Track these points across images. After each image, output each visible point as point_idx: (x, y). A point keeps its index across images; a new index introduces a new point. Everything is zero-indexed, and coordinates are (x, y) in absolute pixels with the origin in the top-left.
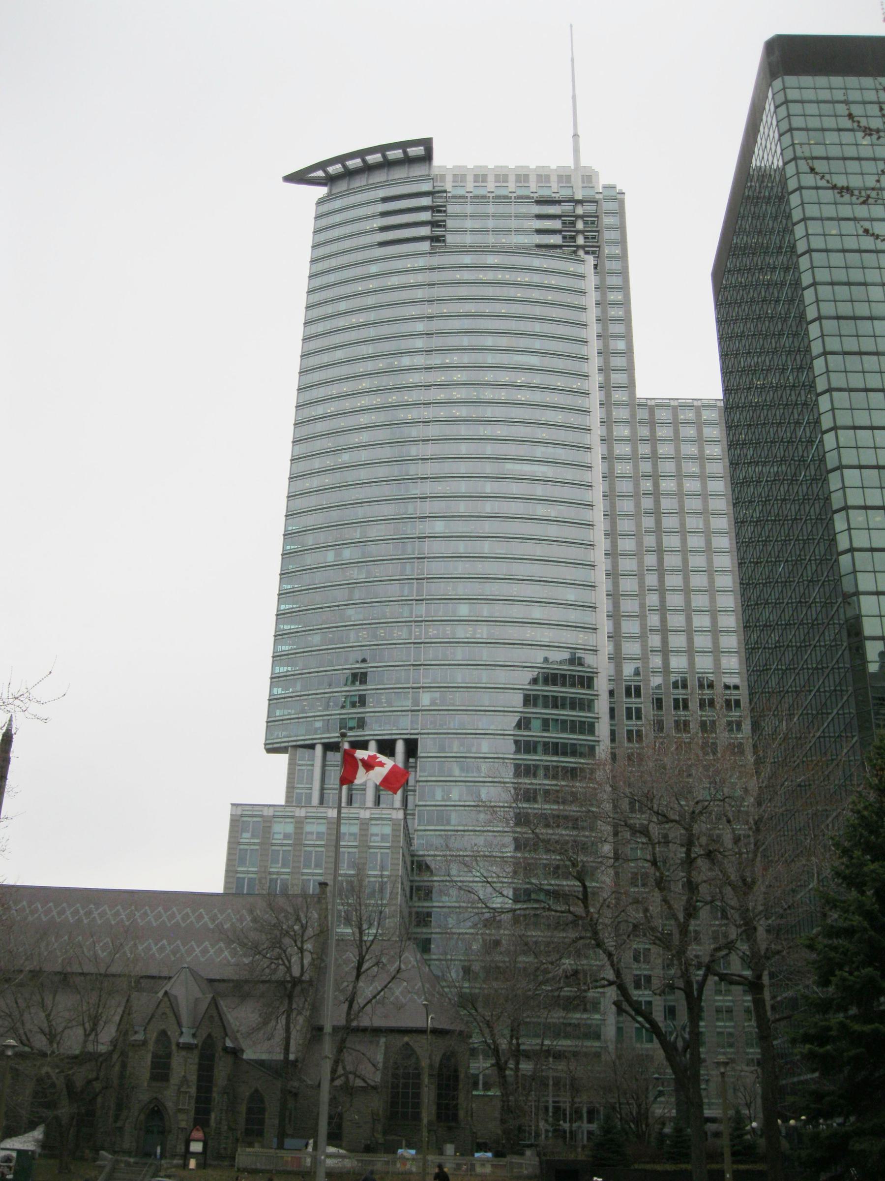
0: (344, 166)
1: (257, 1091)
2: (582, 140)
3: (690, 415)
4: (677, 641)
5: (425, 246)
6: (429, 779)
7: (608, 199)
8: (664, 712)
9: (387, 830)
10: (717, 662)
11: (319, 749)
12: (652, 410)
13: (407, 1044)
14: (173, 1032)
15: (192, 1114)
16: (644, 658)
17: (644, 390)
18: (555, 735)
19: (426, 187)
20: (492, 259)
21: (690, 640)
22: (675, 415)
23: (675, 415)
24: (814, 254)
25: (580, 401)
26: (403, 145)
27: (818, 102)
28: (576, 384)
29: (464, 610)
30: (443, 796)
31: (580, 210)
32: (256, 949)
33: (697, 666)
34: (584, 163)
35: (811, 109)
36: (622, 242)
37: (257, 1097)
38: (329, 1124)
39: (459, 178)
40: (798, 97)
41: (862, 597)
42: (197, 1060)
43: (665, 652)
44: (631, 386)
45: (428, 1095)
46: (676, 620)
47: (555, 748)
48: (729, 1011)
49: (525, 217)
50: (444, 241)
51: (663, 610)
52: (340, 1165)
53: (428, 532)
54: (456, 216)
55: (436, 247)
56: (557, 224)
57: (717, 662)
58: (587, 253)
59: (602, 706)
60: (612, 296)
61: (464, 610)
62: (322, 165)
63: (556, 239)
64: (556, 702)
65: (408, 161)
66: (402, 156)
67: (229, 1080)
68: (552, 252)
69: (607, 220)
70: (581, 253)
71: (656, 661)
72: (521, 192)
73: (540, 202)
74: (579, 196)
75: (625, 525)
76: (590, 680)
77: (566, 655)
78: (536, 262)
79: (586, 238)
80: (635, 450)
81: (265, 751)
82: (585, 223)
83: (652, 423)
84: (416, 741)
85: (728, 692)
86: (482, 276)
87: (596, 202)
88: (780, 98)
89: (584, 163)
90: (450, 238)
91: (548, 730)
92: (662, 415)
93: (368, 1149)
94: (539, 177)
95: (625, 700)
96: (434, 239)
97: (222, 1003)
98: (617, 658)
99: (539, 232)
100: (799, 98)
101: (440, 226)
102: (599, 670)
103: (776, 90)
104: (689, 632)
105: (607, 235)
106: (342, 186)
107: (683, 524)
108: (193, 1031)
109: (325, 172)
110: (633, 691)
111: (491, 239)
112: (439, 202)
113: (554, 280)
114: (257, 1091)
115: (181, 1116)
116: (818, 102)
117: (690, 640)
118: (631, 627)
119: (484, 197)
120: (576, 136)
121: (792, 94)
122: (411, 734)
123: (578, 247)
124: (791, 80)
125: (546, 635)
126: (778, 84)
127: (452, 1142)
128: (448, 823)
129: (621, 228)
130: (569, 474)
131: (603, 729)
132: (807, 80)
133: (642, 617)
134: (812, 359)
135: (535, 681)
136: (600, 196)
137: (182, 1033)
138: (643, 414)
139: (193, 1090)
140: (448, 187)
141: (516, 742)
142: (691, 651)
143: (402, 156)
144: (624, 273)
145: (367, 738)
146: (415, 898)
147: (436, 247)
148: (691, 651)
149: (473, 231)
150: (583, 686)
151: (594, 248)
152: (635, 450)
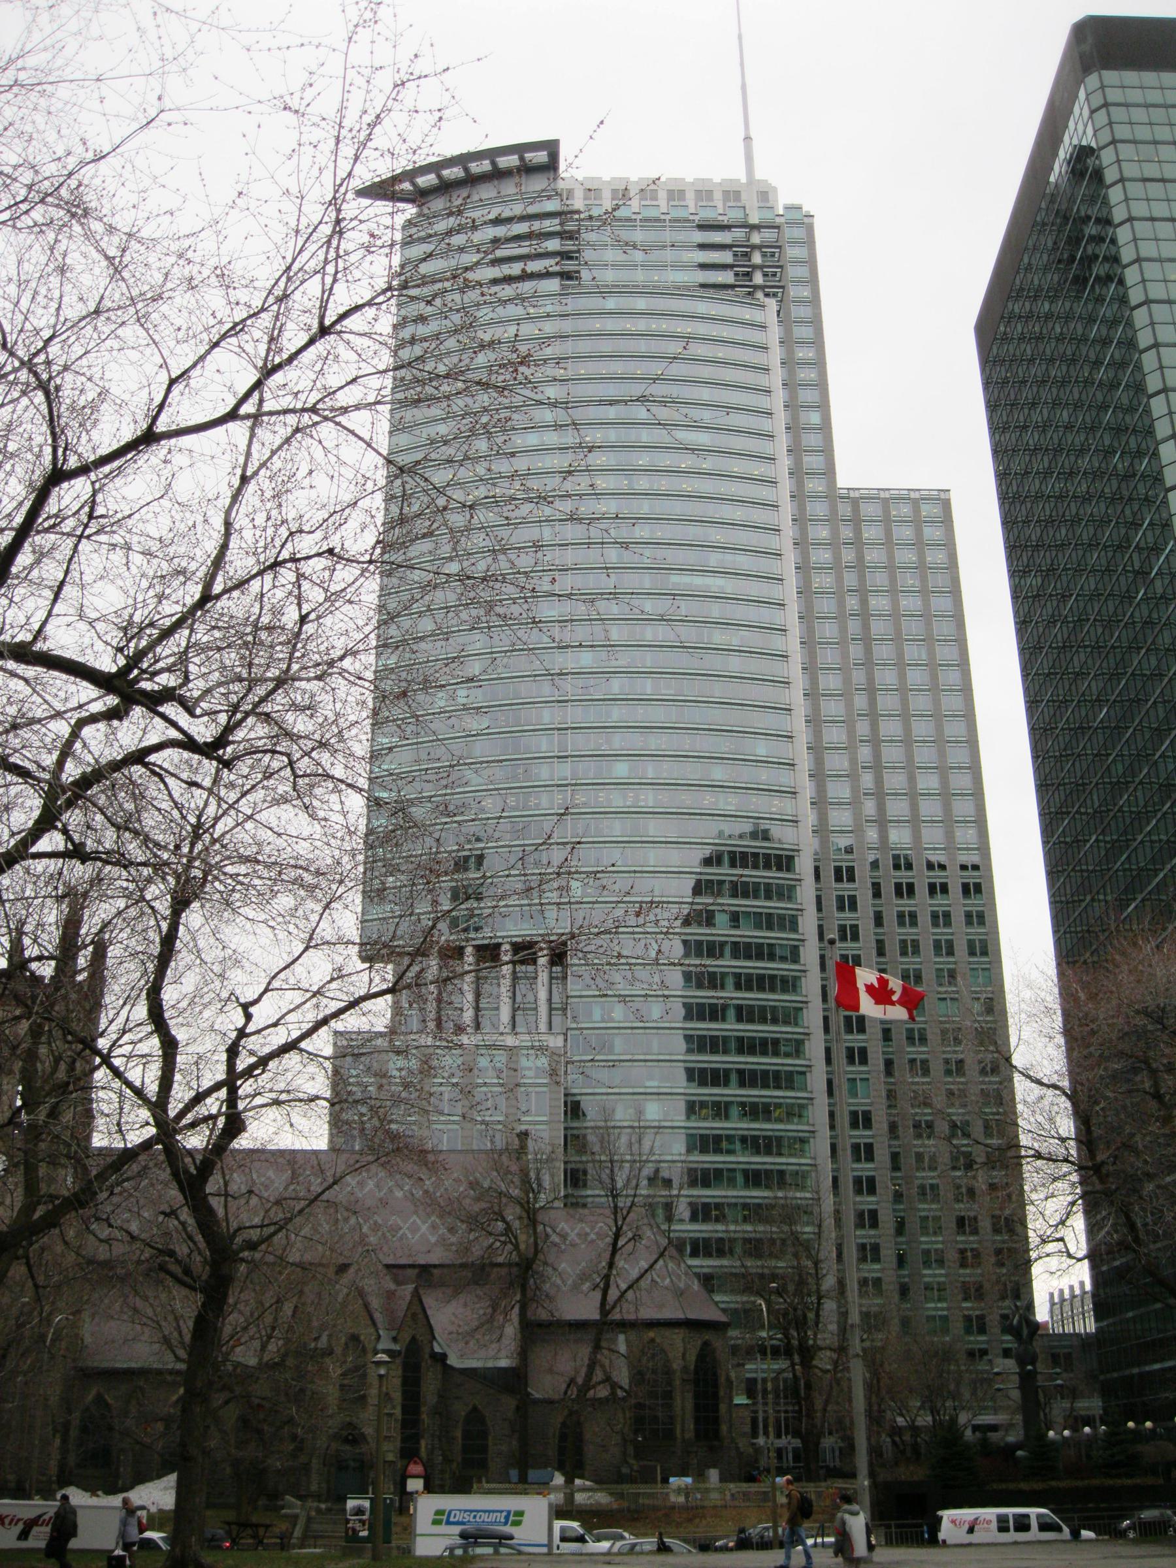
0: (439, 176)
1: (475, 1409)
2: (756, 145)
3: (906, 510)
4: (897, 808)
5: (553, 285)
7: (792, 223)
8: (883, 901)
10: (950, 835)
12: (855, 503)
13: (653, 1340)
14: (366, 1334)
15: (398, 1444)
16: (857, 830)
17: (845, 478)
18: (748, 933)
19: (551, 206)
20: (641, 304)
21: (914, 807)
22: (887, 511)
23: (887, 511)
24: (1153, 306)
25: (763, 493)
26: (520, 149)
27: (1147, 106)
29: (621, 769)
31: (756, 239)
32: (473, 1222)
33: (924, 840)
34: (759, 175)
35: (1139, 114)
36: (813, 281)
37: (475, 1417)
38: (869, 1439)
39: (591, 192)
40: (1121, 100)
42: (400, 1372)
43: (882, 822)
44: (829, 471)
45: (684, 1404)
46: (895, 781)
47: (742, 950)
48: (941, 1288)
49: (685, 246)
50: (579, 278)
51: (877, 766)
52: (592, 1501)
53: (570, 666)
54: (593, 246)
55: (569, 286)
56: (726, 257)
57: (950, 835)
58: (767, 295)
59: (806, 893)
60: (801, 353)
61: (621, 769)
62: (410, 175)
63: (727, 277)
64: (741, 890)
65: (528, 170)
66: (517, 163)
67: (440, 1396)
68: (722, 294)
69: (791, 252)
70: (759, 295)
71: (872, 834)
72: (675, 214)
73: (703, 227)
74: (754, 219)
75: (828, 656)
76: (790, 859)
77: (747, 827)
78: (702, 307)
79: (765, 275)
80: (837, 558)
82: (764, 255)
83: (856, 521)
85: (965, 873)
86: (629, 325)
87: (778, 227)
88: (1097, 100)
89: (759, 175)
90: (585, 275)
91: (737, 927)
92: (869, 510)
93: (620, 1479)
94: (698, 192)
95: (834, 885)
96: (566, 276)
97: (421, 1292)
98: (821, 830)
99: (704, 266)
100: (1161, 101)
101: (571, 258)
103: (1090, 89)
104: (913, 795)
105: (793, 272)
106: (438, 204)
107: (900, 655)
108: (394, 1333)
109: (414, 184)
110: (844, 874)
111: (640, 276)
112: (570, 226)
113: (725, 332)
114: (475, 1409)
115: (386, 1446)
116: (1147, 106)
117: (914, 807)
118: (839, 790)
119: (657, 220)
120: (748, 139)
121: (1114, 95)
123: (756, 287)
124: (1110, 76)
125: (729, 802)
126: (1092, 80)
127: (714, 1467)
128: (611, 1053)
129: (811, 262)
130: (755, 589)
131: (808, 923)
132: (1131, 77)
133: (853, 776)
134: (1158, 444)
135: (707, 862)
136: (782, 220)
137: (379, 1337)
138: (844, 510)
139: (398, 1411)
140: (578, 203)
142: (915, 821)
143: (517, 163)
144: (816, 322)
146: (570, 1150)
147: (569, 286)
148: (915, 821)
149: (615, 266)
150: (779, 869)
151: (776, 288)
152: (837, 558)
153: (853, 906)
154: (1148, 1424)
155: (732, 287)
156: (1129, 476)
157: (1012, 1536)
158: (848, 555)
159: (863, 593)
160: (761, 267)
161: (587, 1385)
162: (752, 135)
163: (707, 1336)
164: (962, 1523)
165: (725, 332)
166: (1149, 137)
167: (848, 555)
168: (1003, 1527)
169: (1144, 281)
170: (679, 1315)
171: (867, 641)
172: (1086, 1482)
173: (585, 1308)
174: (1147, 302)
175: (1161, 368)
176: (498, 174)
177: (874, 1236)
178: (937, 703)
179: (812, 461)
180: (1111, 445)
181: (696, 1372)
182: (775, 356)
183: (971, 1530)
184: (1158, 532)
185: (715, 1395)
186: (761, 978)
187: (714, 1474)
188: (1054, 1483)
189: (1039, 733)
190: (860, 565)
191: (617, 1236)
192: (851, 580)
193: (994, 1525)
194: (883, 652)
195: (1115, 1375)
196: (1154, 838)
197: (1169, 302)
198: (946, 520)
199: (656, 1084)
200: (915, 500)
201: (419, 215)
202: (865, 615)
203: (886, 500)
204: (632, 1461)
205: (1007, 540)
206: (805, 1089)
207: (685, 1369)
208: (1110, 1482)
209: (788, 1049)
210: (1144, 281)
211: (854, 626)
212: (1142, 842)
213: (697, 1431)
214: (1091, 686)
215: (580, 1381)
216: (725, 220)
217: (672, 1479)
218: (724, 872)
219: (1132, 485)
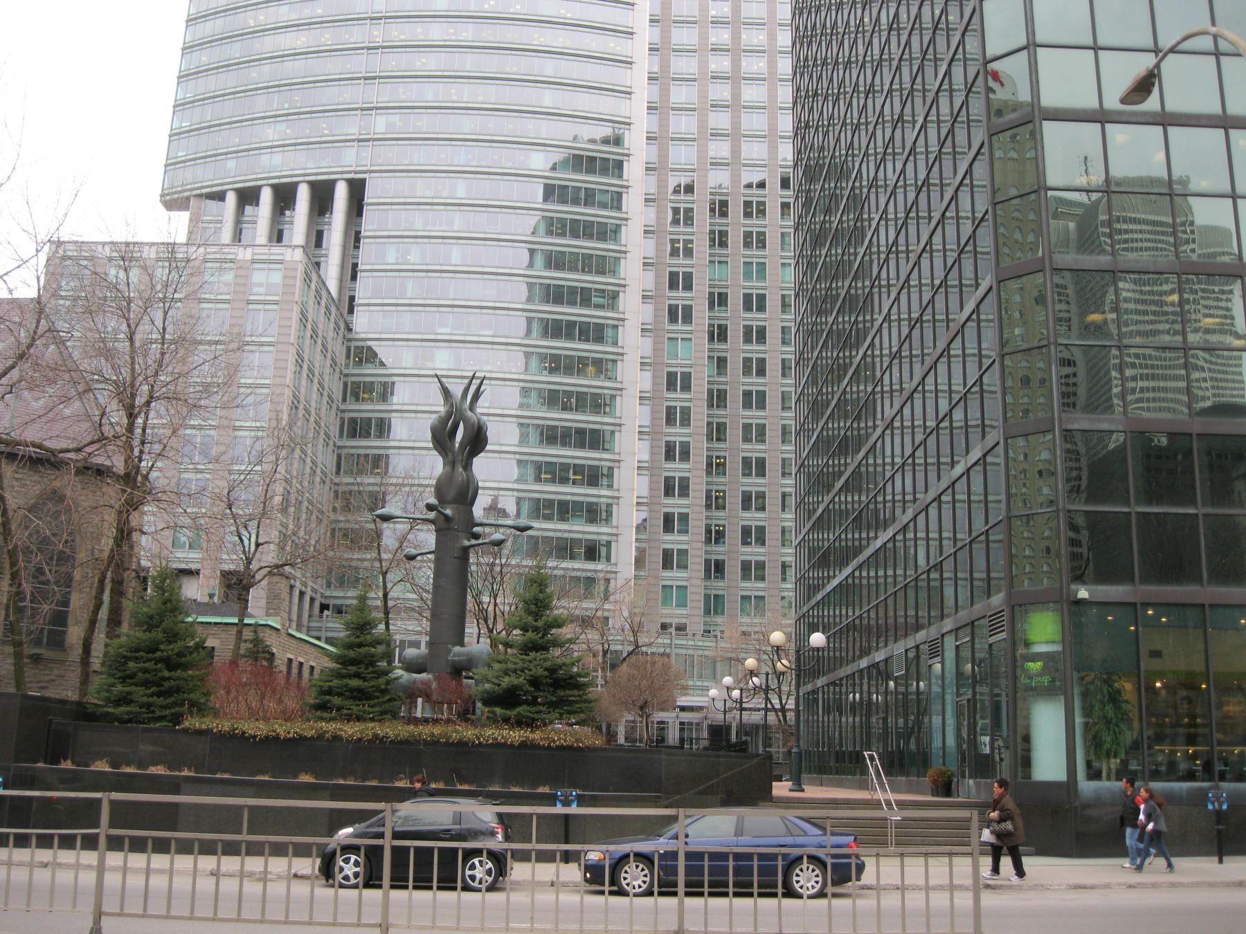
6: (378, 233)
9: (276, 277)
11: (231, 198)
28: (613, 45)
30: (397, 258)
41: (1039, 50)
81: (164, 209)
84: (363, 181)
102: (630, 184)
122: (356, 173)
141: (530, 286)
145: (295, 179)
153: (689, 220)
177: (681, 616)
186: (573, 291)
197: (1226, 123)
199: (448, 330)
206: (615, 343)
209: (600, 301)
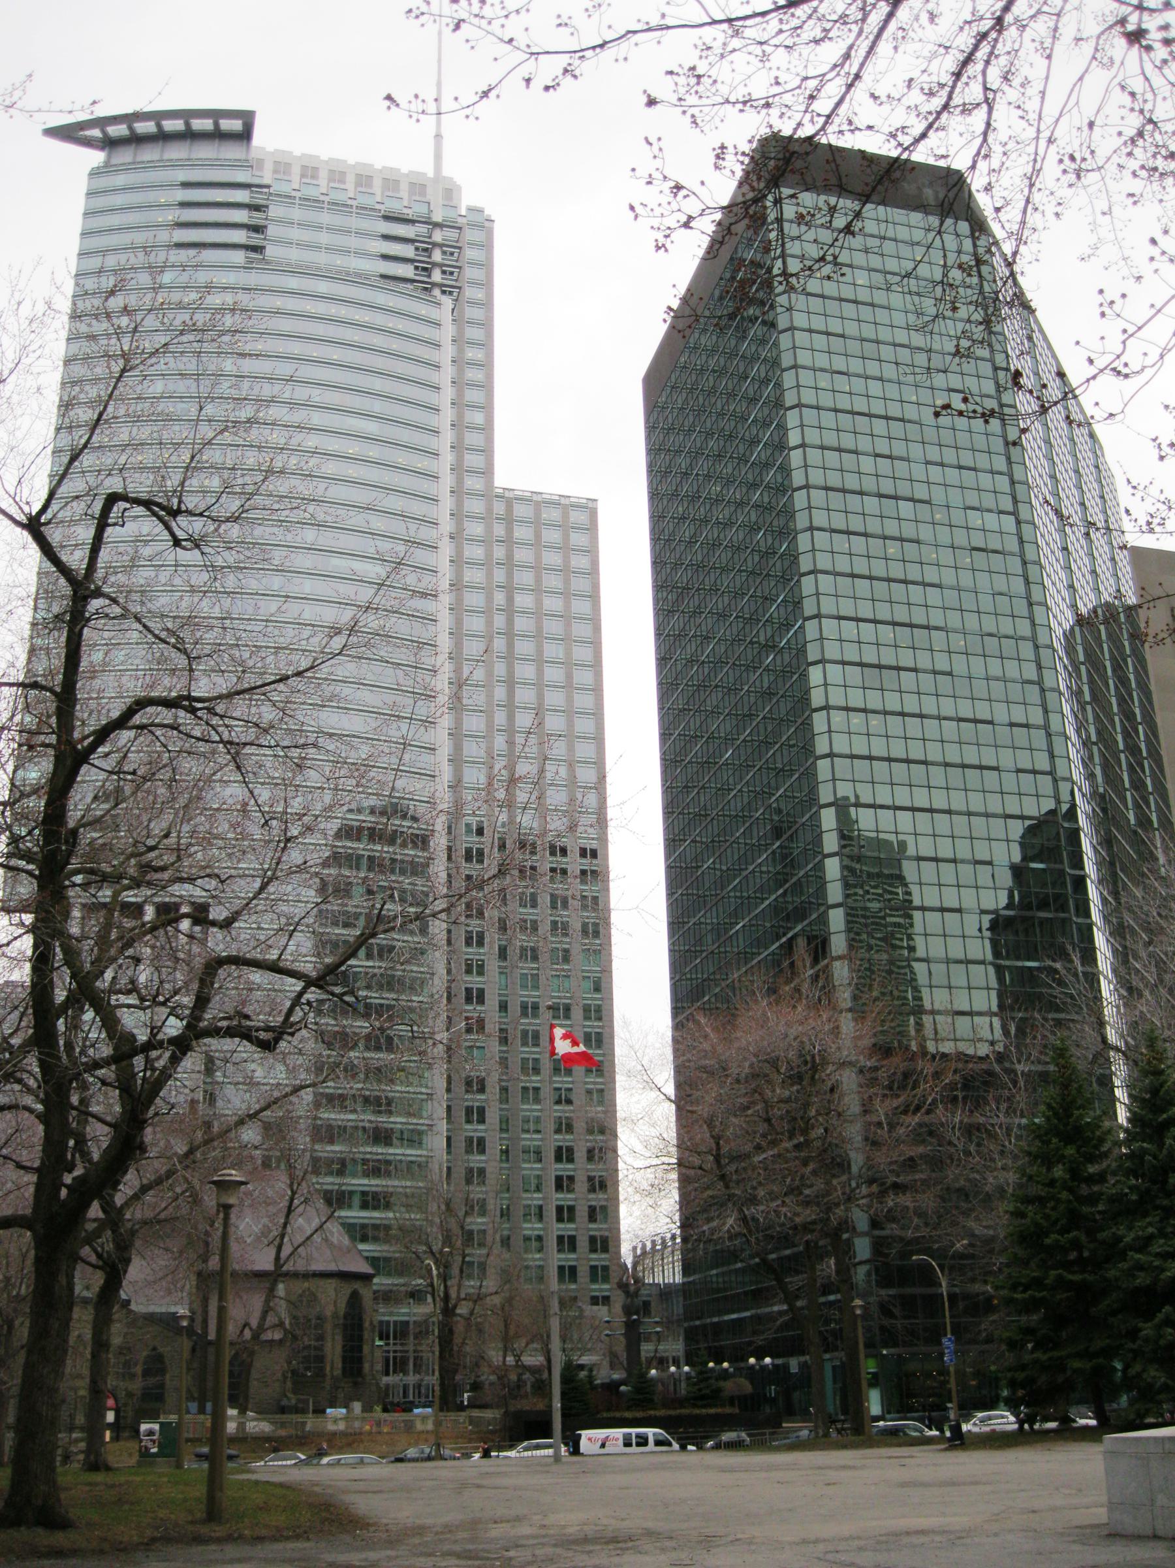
2: (446, 143)
5: (239, 257)
7: (473, 225)
17: (503, 479)
20: (323, 287)
25: (425, 486)
31: (438, 236)
34: (447, 171)
39: (282, 166)
44: (488, 472)
56: (408, 251)
58: (444, 292)
60: (471, 354)
62: (102, 122)
63: (407, 271)
69: (470, 254)
70: (437, 292)
73: (387, 218)
74: (437, 217)
78: (381, 298)
80: (489, 554)
83: (509, 520)
92: (520, 511)
99: (385, 257)
105: (470, 273)
106: (125, 156)
109: (103, 132)
123: (434, 285)
136: (464, 221)
152: (489, 554)
154: (768, 1360)
155: (413, 281)
156: (769, 553)
157: (634, 1449)
158: (499, 552)
159: (510, 589)
160: (441, 265)
161: (261, 1328)
162: (444, 132)
163: (357, 1285)
164: (596, 1440)
165: (401, 325)
166: (823, 328)
167: (499, 552)
168: (627, 1444)
169: (798, 386)
170: (332, 1267)
171: (510, 635)
172: (678, 1411)
173: (264, 1261)
174: (799, 405)
175: (806, 466)
176: (190, 135)
178: (570, 700)
179: (473, 460)
180: (756, 523)
181: (345, 1317)
182: (447, 353)
183: (603, 1446)
184: (790, 609)
185: (361, 1338)
187: (357, 1406)
188: (652, 1412)
189: (671, 762)
190: (509, 564)
191: (292, 1200)
192: (500, 576)
193: (621, 1442)
194: (524, 647)
195: (698, 1323)
196: (764, 869)
198: (592, 528)
200: (564, 505)
201: (107, 164)
202: (510, 611)
203: (538, 502)
204: (290, 1395)
205: (655, 581)
207: (335, 1315)
208: (697, 1411)
210: (798, 386)
211: (499, 621)
212: (753, 871)
213: (344, 1369)
214: (718, 726)
215: (254, 1323)
216: (410, 213)
217: (329, 1411)
218: (361, 847)
219: (771, 563)
